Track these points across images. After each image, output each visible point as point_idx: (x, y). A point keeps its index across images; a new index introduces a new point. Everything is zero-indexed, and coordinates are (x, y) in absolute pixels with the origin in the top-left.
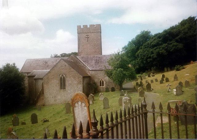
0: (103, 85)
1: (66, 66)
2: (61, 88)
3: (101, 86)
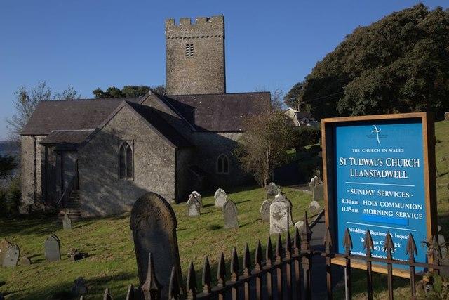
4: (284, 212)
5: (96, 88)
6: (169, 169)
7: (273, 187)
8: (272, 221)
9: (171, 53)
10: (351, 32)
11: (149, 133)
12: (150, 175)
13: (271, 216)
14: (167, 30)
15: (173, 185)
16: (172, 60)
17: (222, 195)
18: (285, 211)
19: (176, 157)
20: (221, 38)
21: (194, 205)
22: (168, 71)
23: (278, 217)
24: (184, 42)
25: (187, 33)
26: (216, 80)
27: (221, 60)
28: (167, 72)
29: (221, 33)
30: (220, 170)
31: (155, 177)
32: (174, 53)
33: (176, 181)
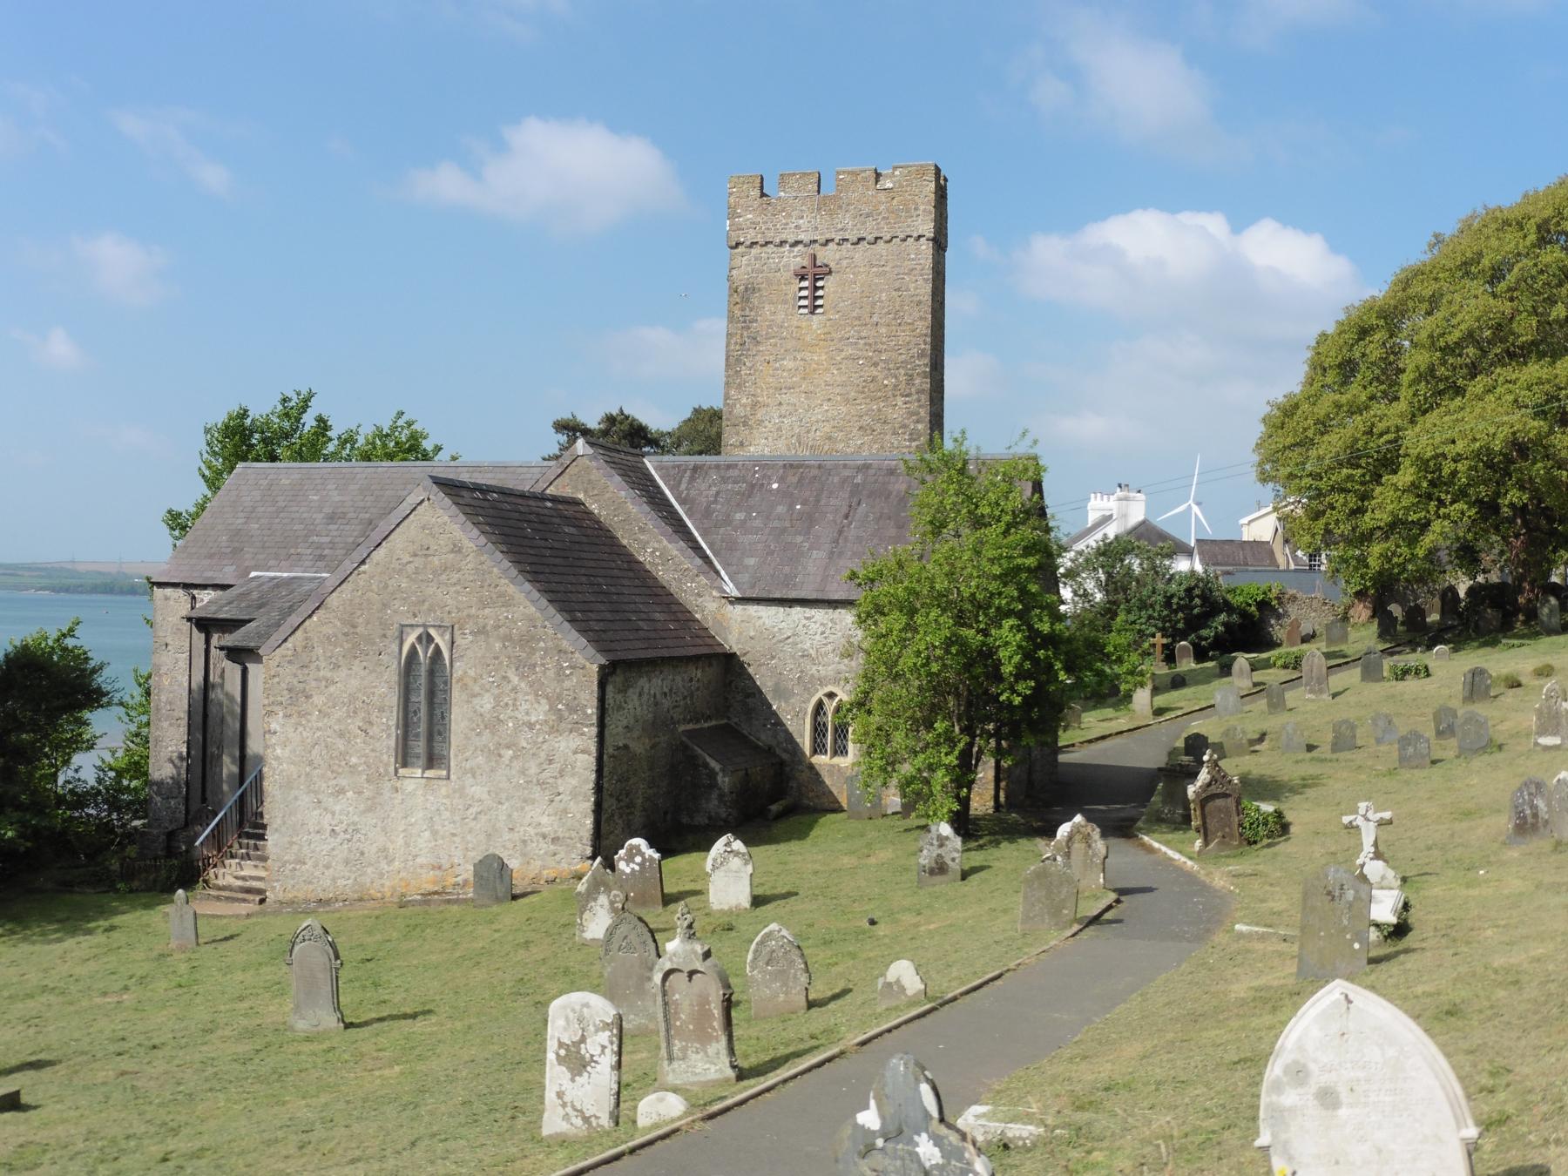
0: (840, 750)
1: (457, 549)
2: (405, 759)
3: (818, 748)
4: (599, 1044)
5: (565, 415)
6: (575, 741)
7: (942, 841)
8: (556, 1076)
9: (743, 297)
10: (1449, 228)
11: (508, 603)
12: (506, 760)
13: (551, 1056)
14: (732, 215)
15: (588, 805)
16: (747, 323)
17: (736, 862)
18: (604, 1037)
19: (602, 700)
20: (926, 248)
21: (603, 899)
22: (733, 363)
23: (577, 1062)
24: (795, 259)
25: (805, 225)
26: (900, 401)
27: (924, 326)
28: (728, 365)
29: (927, 228)
30: (818, 748)
31: (523, 772)
32: (755, 301)
33: (599, 789)
